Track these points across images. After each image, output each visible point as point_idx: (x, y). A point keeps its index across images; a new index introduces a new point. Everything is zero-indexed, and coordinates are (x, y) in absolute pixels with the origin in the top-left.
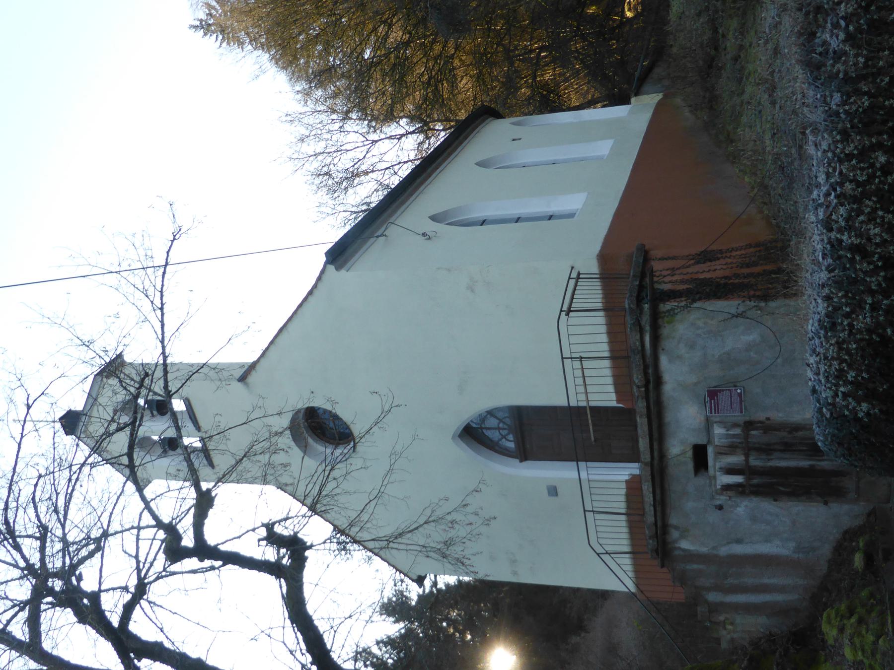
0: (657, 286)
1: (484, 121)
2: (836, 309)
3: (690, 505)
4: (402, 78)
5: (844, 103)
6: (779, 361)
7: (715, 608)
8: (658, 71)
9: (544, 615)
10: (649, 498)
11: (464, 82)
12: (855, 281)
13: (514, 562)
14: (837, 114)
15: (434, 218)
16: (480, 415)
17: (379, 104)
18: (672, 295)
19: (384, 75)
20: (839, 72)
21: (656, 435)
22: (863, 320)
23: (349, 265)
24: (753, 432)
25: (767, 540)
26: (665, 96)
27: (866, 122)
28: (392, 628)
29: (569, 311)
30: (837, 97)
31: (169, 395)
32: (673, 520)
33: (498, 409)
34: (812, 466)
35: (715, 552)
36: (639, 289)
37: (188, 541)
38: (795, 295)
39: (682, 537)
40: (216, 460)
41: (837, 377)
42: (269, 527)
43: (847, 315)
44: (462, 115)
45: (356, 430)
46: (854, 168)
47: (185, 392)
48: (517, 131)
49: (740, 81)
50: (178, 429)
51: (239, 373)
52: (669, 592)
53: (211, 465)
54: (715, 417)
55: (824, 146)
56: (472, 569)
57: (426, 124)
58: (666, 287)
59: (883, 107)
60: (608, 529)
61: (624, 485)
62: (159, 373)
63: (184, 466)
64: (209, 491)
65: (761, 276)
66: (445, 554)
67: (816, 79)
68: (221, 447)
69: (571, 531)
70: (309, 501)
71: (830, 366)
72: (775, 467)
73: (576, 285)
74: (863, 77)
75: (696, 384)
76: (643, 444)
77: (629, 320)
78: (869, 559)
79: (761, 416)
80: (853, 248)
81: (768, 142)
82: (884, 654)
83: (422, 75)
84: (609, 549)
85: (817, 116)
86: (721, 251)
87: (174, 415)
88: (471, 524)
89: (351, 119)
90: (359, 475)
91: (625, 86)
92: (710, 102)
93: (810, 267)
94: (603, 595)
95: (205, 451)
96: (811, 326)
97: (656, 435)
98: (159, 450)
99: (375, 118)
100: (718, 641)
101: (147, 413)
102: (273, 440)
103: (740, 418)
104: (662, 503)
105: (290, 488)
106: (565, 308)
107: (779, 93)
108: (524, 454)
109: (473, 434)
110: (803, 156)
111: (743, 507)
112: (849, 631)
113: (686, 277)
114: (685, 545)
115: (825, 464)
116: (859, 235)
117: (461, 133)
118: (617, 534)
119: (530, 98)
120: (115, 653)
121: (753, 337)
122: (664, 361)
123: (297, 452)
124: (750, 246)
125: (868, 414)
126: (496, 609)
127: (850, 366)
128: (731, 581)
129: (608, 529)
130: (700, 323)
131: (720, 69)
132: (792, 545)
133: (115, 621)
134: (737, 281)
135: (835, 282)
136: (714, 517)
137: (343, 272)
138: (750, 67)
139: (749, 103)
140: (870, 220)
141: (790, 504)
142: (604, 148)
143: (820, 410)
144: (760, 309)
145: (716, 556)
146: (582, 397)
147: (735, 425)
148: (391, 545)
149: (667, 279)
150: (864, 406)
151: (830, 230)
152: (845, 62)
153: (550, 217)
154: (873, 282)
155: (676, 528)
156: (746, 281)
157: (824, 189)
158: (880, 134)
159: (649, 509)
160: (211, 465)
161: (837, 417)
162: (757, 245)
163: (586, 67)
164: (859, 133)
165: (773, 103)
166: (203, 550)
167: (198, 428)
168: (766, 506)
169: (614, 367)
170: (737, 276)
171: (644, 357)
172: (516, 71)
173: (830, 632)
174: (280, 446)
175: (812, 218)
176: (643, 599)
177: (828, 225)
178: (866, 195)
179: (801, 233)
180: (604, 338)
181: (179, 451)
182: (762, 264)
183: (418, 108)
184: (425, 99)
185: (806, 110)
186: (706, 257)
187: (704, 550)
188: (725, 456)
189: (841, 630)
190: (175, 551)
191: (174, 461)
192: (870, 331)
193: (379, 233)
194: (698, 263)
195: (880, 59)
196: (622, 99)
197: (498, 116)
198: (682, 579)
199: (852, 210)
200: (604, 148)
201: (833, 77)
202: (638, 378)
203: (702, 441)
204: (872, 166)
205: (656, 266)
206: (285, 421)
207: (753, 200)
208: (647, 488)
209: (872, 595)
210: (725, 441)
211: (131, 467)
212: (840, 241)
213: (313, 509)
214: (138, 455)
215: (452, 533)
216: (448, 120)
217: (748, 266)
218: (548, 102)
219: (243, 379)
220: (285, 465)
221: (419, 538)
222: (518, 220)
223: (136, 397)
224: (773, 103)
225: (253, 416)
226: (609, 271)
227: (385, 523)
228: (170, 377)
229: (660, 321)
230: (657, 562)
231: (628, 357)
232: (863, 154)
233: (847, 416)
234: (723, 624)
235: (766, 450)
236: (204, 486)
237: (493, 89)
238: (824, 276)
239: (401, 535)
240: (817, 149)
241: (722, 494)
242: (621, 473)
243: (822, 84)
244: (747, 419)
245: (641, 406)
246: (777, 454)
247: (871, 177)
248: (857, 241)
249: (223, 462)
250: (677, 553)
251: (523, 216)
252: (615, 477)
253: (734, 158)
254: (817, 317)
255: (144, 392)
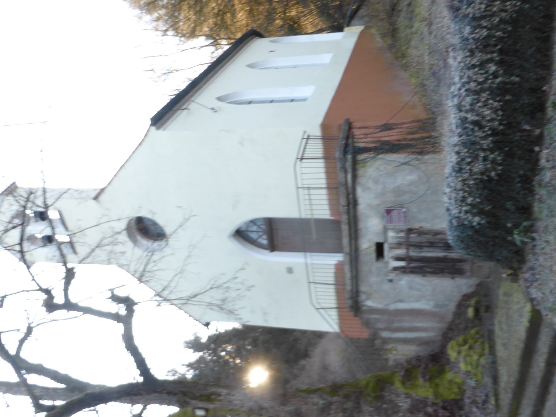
0: (357, 145)
1: (252, 39)
2: (463, 160)
3: (373, 279)
4: (201, 11)
5: (472, 33)
6: (429, 192)
7: (386, 341)
8: (362, 12)
9: (284, 346)
10: (348, 275)
11: (240, 14)
12: (474, 143)
13: (265, 314)
14: (467, 39)
15: (220, 99)
16: (246, 223)
17: (186, 26)
18: (365, 150)
19: (190, 8)
20: (469, 14)
21: (353, 236)
22: (478, 167)
23: (165, 126)
24: (412, 235)
25: (418, 300)
26: (366, 28)
27: (484, 45)
28: (194, 356)
29: (302, 159)
30: (468, 29)
31: (47, 207)
32: (363, 288)
33: (256, 219)
34: (446, 256)
35: (387, 308)
36: (346, 146)
37: (59, 299)
38: (439, 152)
39: (368, 298)
40: (78, 248)
41: (462, 201)
42: (112, 290)
43: (469, 164)
44: (239, 35)
45: (168, 230)
46: (476, 74)
47: (58, 204)
48: (273, 46)
49: (411, 19)
50: (53, 228)
51: (94, 194)
52: (360, 332)
53: (75, 252)
54: (390, 226)
55: (459, 59)
56: (239, 317)
57: (216, 40)
58: (362, 145)
59: (494, 37)
60: (324, 294)
61: (333, 267)
62: (40, 193)
63: (57, 253)
64: (72, 269)
65: (419, 141)
66: (223, 308)
67: (456, 17)
68: (82, 240)
69: (302, 296)
70: (138, 275)
71: (458, 194)
72: (426, 258)
73: (306, 143)
74: (483, 17)
75: (378, 205)
76: (345, 241)
77: (339, 165)
78: (477, 311)
79: (416, 226)
80: (475, 123)
81: (426, 58)
82: (483, 367)
83: (213, 9)
84: (324, 305)
85: (456, 40)
86: (396, 124)
87: (51, 222)
88: (238, 289)
89: (167, 35)
90: (168, 258)
91: (342, 21)
92: (393, 32)
93: (449, 134)
94: (320, 335)
95: (71, 244)
96: (448, 170)
97: (353, 236)
98: (41, 244)
99: (184, 36)
100: (387, 360)
101: (33, 220)
102: (116, 236)
103: (405, 227)
104: (356, 278)
105: (126, 267)
106: (300, 157)
107: (434, 27)
108: (273, 247)
109: (241, 234)
110: (446, 66)
111: (405, 281)
112: (463, 353)
113: (375, 139)
114: (370, 303)
115: (453, 255)
116: (478, 115)
117: (238, 46)
118: (329, 297)
119: (282, 26)
120: (13, 370)
121: (413, 177)
122: (359, 191)
123: (130, 244)
124: (413, 122)
125: (479, 224)
126: (255, 343)
127: (470, 194)
128: (396, 325)
129: (324, 294)
130: (382, 168)
131: (400, 11)
132: (432, 303)
133: (12, 352)
134: (405, 143)
135: (463, 143)
136: (387, 286)
137: (161, 132)
138: (417, 11)
139: (416, 33)
140: (485, 106)
141: (433, 278)
142: (326, 58)
143: (450, 222)
144: (418, 160)
145: (387, 310)
146: (309, 212)
147: (402, 231)
148: (189, 302)
149: (363, 140)
150: (477, 219)
151: (461, 111)
152: (473, 8)
153: (292, 100)
154: (486, 143)
155: (364, 293)
156: (411, 142)
157: (458, 86)
158: (492, 52)
159: (348, 282)
160: (75, 252)
161: (461, 226)
162: (418, 121)
163: (318, 8)
164: (480, 52)
165: (430, 33)
166: (69, 306)
167: (66, 228)
168: (418, 280)
169: (329, 194)
170: (405, 139)
171: (347, 188)
172: (274, 9)
173: (452, 354)
174: (120, 241)
175: (450, 104)
176: (343, 335)
177: (459, 108)
178: (482, 90)
179: (443, 113)
180: (323, 176)
181: (54, 243)
182: (420, 133)
183: (211, 29)
184: (216, 24)
185: (449, 36)
186: (387, 127)
187: (380, 306)
188: (395, 250)
189: (459, 353)
190: (50, 306)
191: (51, 250)
192: (482, 173)
193: (183, 107)
194: (381, 131)
195: (494, 6)
196: (339, 29)
197: (261, 36)
198: (367, 324)
199: (474, 99)
200: (326, 58)
201: (466, 16)
202: (343, 201)
203: (381, 240)
204: (487, 72)
205: (356, 132)
206: (122, 225)
207: (416, 93)
208: (347, 268)
209: (477, 333)
210: (395, 241)
211: (22, 252)
212: (466, 118)
213: (140, 279)
214: (26, 246)
215: (227, 295)
216: (229, 38)
217: (412, 133)
218: (293, 29)
219: (96, 198)
220: (123, 253)
221: (206, 298)
222: (272, 101)
223: (25, 207)
224: (430, 33)
225: (102, 221)
226: (327, 136)
227: (186, 289)
228: (48, 195)
229: (358, 166)
230: (352, 314)
231: (337, 188)
232: (482, 65)
233: (466, 225)
234: (390, 350)
235: (419, 246)
236: (69, 266)
237: (259, 19)
238: (455, 139)
239: (195, 296)
240: (456, 60)
241: (391, 273)
242: (331, 260)
243: (460, 20)
244: (409, 227)
245: (344, 218)
246: (426, 249)
247: (487, 79)
248: (476, 118)
249: (83, 251)
250: (364, 308)
251: (276, 99)
252: (327, 263)
253: (406, 67)
254: (451, 164)
255: (29, 205)
